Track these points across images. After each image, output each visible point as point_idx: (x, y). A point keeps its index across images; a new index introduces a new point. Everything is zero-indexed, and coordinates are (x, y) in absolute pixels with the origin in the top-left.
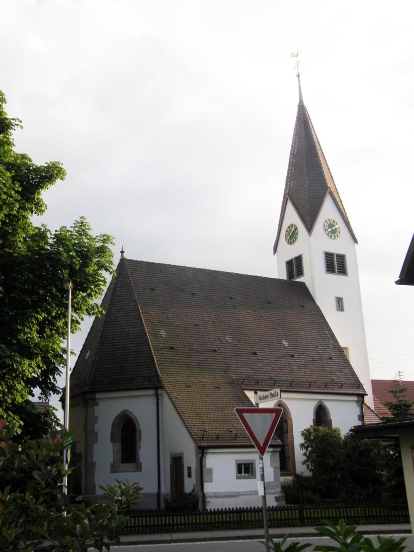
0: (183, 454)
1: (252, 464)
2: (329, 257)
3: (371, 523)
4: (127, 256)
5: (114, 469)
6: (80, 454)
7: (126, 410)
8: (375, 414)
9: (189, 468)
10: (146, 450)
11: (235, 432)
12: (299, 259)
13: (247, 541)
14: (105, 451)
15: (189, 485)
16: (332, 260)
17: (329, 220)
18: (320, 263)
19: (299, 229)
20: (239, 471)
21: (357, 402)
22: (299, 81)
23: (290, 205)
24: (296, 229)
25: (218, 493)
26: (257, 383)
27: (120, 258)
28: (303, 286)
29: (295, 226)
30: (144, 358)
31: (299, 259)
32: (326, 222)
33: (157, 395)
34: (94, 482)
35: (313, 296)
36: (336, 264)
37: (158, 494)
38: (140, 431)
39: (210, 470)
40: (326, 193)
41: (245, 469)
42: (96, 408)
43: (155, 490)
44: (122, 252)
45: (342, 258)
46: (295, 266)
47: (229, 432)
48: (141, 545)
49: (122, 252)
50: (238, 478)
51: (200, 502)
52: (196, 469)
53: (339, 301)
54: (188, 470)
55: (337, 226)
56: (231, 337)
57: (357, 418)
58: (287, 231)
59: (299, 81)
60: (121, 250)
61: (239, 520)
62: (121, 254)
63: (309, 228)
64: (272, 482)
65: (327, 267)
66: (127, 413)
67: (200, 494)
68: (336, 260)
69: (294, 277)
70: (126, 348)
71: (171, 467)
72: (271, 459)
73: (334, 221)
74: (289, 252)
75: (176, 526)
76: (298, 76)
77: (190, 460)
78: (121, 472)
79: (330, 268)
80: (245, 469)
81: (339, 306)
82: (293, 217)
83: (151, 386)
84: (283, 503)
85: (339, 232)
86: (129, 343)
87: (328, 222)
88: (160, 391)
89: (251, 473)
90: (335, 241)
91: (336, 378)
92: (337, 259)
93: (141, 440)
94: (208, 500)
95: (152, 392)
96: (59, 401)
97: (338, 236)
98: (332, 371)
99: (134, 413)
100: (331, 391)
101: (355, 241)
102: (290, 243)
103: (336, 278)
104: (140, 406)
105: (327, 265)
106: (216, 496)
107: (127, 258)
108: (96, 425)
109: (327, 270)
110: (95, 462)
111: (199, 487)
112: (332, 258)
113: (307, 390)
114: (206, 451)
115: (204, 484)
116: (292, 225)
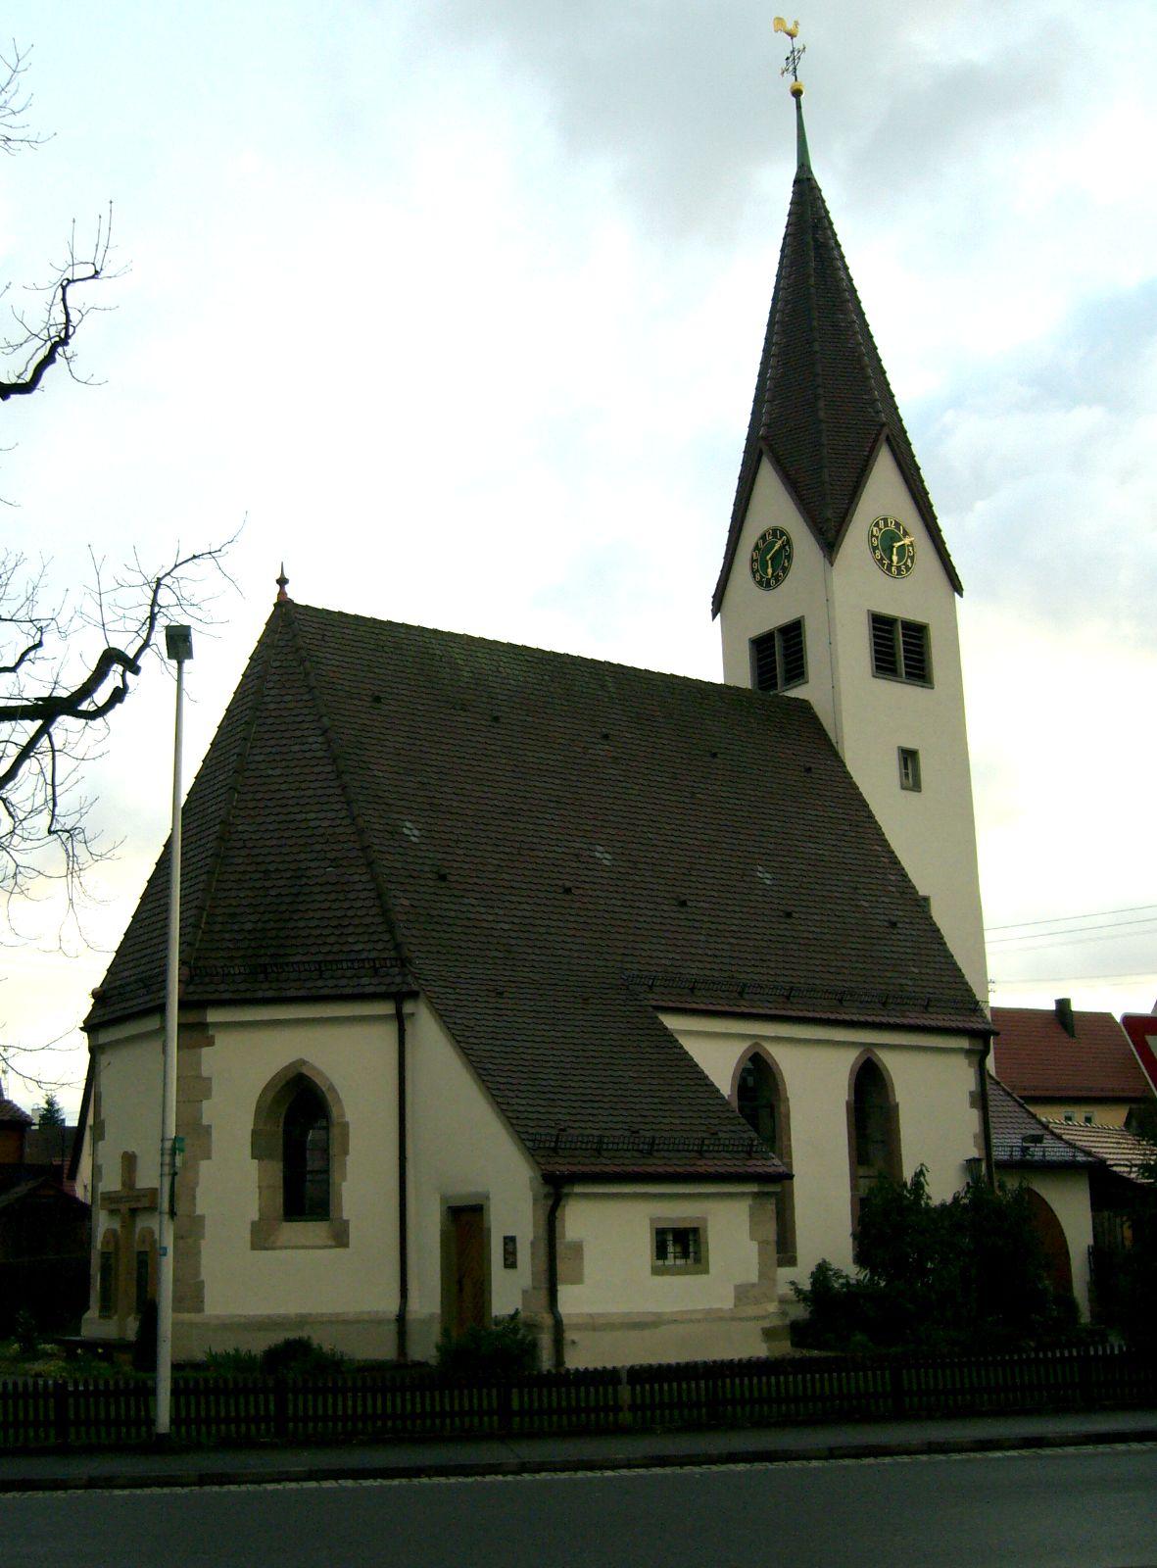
0: (487, 1198)
1: (695, 1231)
2: (882, 626)
3: (1104, 1409)
4: (298, 595)
5: (261, 1237)
6: (153, 1193)
7: (303, 1062)
8: (1004, 1090)
9: (510, 1242)
10: (362, 1182)
11: (648, 1134)
12: (793, 633)
13: (758, 1466)
14: (233, 1181)
15: (508, 1293)
16: (919, 638)
17: (885, 520)
18: (855, 648)
19: (795, 545)
20: (661, 1252)
21: (968, 1052)
22: (799, 107)
23: (768, 479)
24: (788, 542)
25: (602, 1315)
26: (692, 989)
27: (275, 601)
28: (804, 710)
29: (783, 533)
30: (359, 904)
31: (793, 633)
32: (877, 525)
33: (400, 1019)
34: (197, 1273)
35: (834, 741)
36: (905, 651)
37: (401, 1319)
38: (345, 1126)
39: (577, 1249)
40: (876, 441)
41: (679, 1245)
42: (205, 1050)
43: (392, 1307)
44: (282, 582)
45: (917, 633)
46: (779, 653)
47: (627, 1133)
48: (425, 1480)
49: (282, 582)
50: (656, 1271)
51: (546, 1340)
52: (533, 1244)
53: (909, 757)
54: (505, 1244)
55: (907, 541)
56: (610, 850)
57: (966, 1099)
58: (757, 547)
59: (799, 107)
60: (278, 576)
61: (686, 1400)
62: (278, 587)
63: (830, 542)
64: (753, 1285)
65: (877, 659)
66: (305, 1070)
67: (547, 1320)
68: (901, 638)
69: (776, 684)
70: (299, 873)
71: (444, 1233)
72: (751, 1216)
73: (897, 525)
74: (770, 611)
75: (517, 1419)
76: (797, 94)
77: (513, 1212)
78: (281, 1248)
79: (884, 665)
80: (679, 1245)
81: (907, 775)
82: (775, 506)
83: (383, 988)
84: (784, 1348)
85: (912, 558)
86: (309, 856)
87: (881, 523)
88: (408, 1008)
89: (692, 1255)
90: (898, 582)
91: (910, 983)
92: (904, 635)
93: (346, 1152)
94: (569, 1335)
95: (387, 1008)
96: (81, 1029)
97: (908, 569)
98: (893, 961)
99: (328, 1073)
100: (898, 1021)
101: (956, 586)
102: (765, 584)
103: (899, 693)
104: (349, 1054)
105: (876, 651)
106: (595, 1325)
107: (296, 601)
108: (205, 1104)
109: (877, 667)
110: (202, 1218)
111: (542, 1296)
112: (891, 640)
113: (832, 1017)
114: (566, 1190)
115: (559, 1288)
116: (775, 531)
